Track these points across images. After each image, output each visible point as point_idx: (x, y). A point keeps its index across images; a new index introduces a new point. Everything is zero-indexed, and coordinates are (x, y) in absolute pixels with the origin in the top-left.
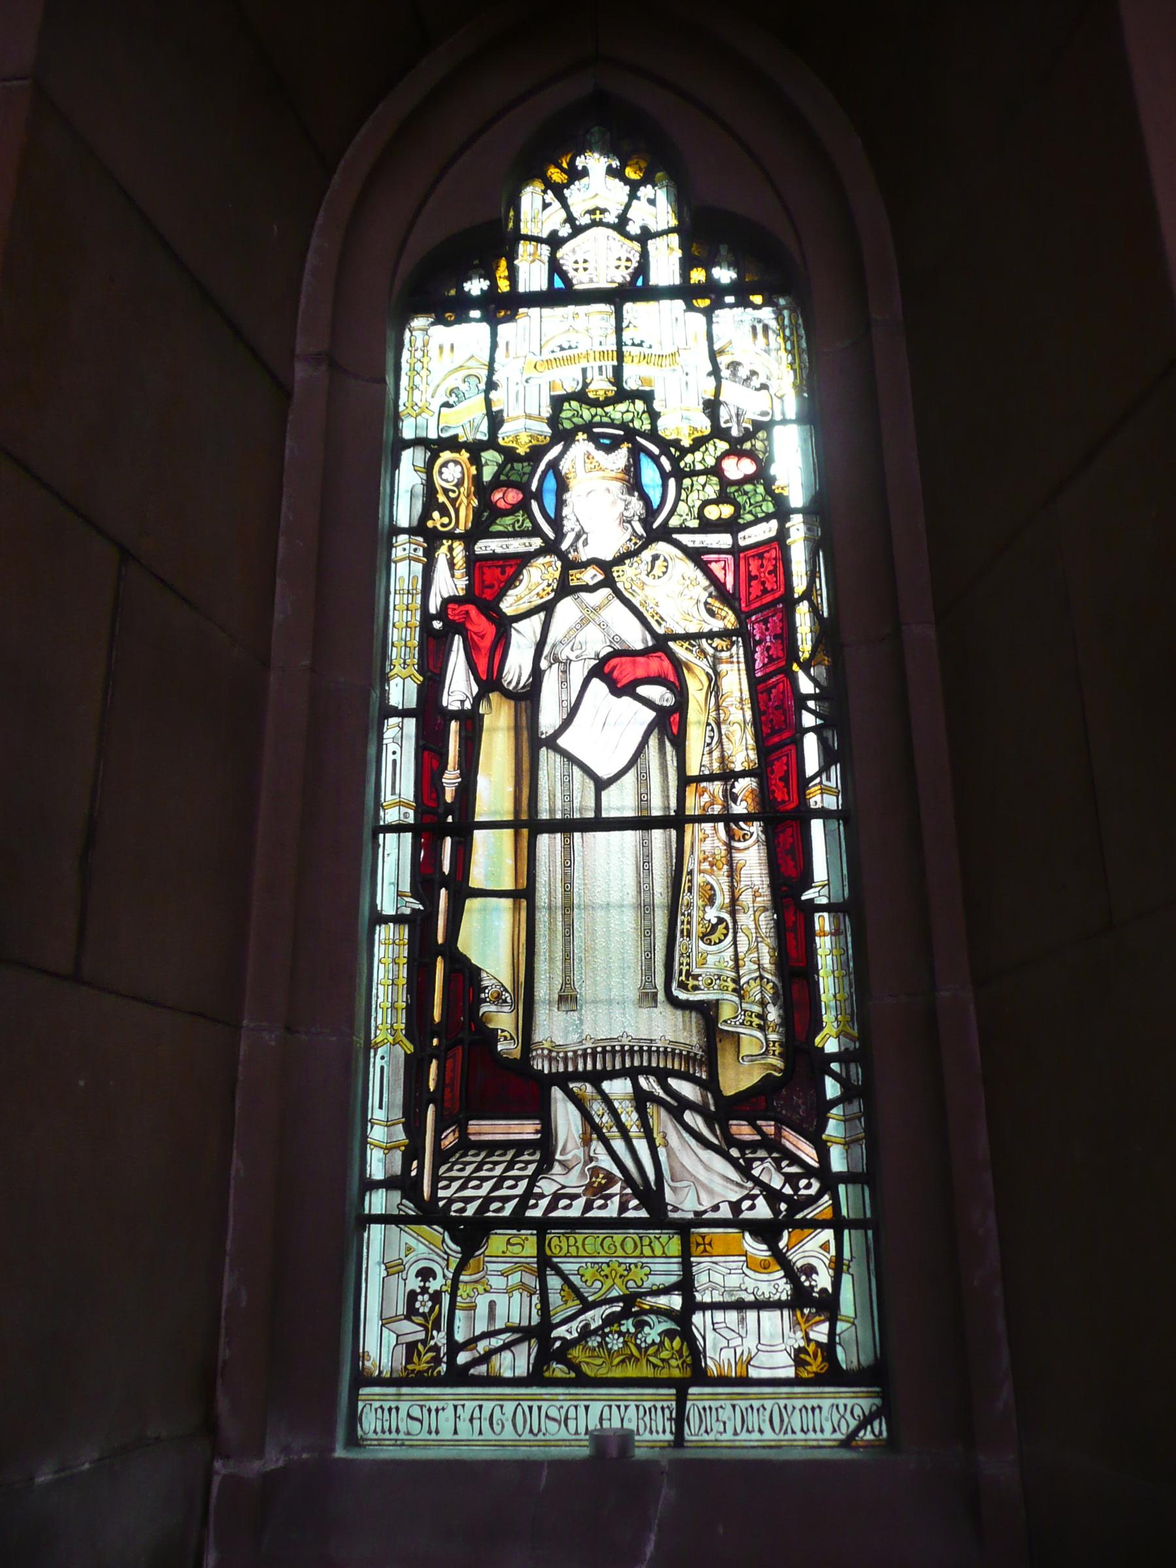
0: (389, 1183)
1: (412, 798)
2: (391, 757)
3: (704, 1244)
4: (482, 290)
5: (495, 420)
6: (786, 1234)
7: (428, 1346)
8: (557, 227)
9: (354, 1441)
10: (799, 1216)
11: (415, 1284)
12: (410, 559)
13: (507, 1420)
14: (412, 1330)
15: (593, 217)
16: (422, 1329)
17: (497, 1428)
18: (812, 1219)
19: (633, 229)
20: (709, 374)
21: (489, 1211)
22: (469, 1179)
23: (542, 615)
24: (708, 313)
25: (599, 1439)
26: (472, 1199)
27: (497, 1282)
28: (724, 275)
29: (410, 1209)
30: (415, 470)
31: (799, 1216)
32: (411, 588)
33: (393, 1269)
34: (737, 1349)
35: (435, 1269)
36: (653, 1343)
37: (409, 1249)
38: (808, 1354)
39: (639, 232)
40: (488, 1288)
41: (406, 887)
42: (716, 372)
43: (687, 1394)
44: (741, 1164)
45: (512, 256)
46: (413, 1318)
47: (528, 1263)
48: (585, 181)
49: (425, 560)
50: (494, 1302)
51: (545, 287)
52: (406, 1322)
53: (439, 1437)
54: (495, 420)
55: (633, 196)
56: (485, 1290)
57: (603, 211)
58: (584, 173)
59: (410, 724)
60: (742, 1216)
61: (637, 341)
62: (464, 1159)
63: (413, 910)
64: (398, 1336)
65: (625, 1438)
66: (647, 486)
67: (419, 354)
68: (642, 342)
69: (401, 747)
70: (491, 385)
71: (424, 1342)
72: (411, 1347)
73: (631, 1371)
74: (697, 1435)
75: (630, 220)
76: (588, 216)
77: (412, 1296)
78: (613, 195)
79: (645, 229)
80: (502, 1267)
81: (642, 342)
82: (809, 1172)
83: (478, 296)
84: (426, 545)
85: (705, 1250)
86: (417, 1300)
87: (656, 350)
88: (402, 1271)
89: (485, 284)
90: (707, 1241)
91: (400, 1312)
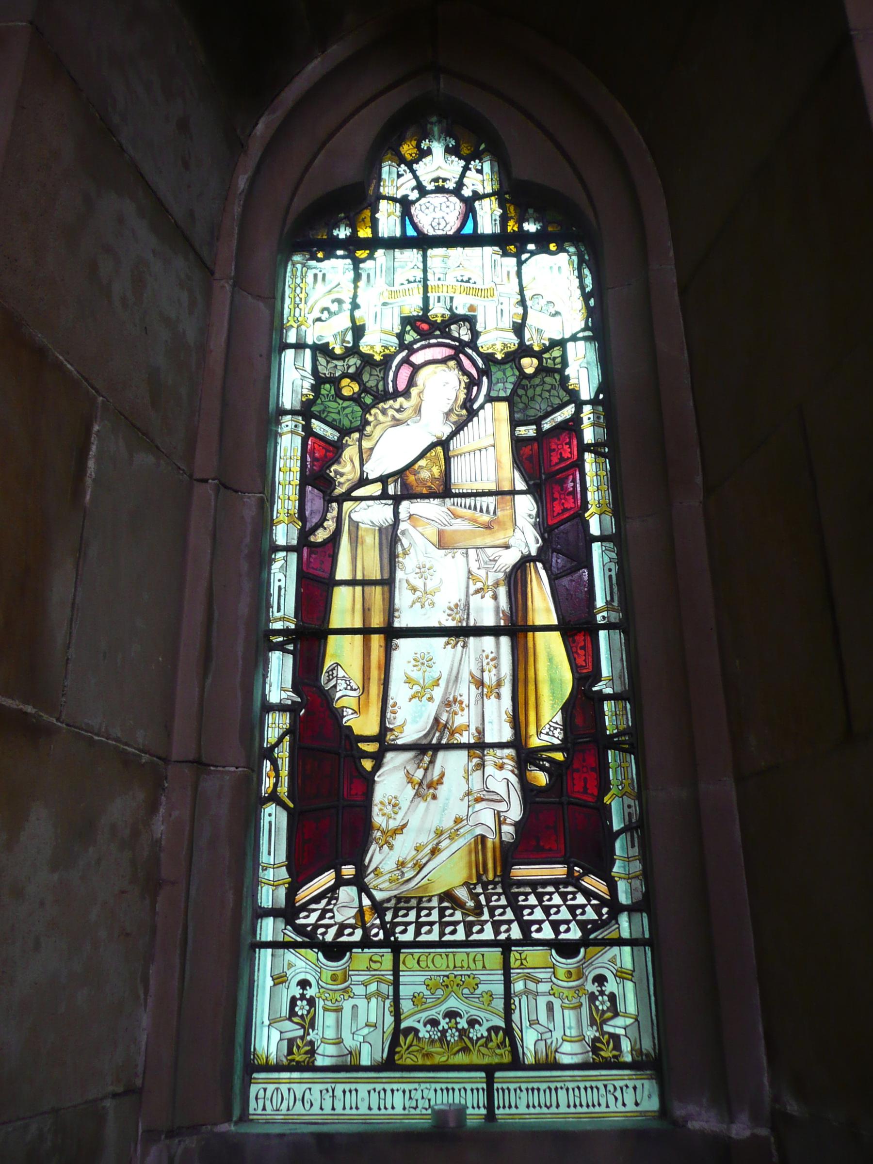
0: (274, 912)
1: (293, 615)
2: (277, 584)
3: (521, 960)
4: (346, 235)
6: (582, 950)
7: (305, 1042)
8: (408, 192)
9: (244, 1117)
10: (592, 936)
11: (297, 992)
12: (292, 432)
13: (316, 1100)
14: (293, 1030)
15: (436, 184)
16: (299, 1027)
17: (307, 1106)
18: (603, 939)
19: (467, 192)
25: (440, 1116)
27: (359, 990)
29: (292, 936)
30: (296, 368)
31: (592, 936)
32: (292, 454)
33: (279, 980)
34: (547, 1041)
35: (312, 982)
36: (482, 1037)
37: (290, 965)
38: (603, 1043)
39: (471, 194)
40: (352, 995)
41: (288, 684)
42: (523, 302)
45: (375, 210)
46: (293, 1019)
47: (383, 975)
48: (429, 158)
49: (303, 433)
50: (356, 1006)
51: (398, 234)
52: (287, 1022)
53: (359, 1112)
55: (466, 168)
56: (349, 997)
57: (444, 180)
58: (429, 152)
59: (293, 557)
60: (560, 937)
61: (465, 279)
63: (293, 702)
64: (281, 1033)
65: (460, 1111)
67: (298, 281)
68: (470, 279)
69: (285, 576)
70: (355, 306)
71: (302, 1038)
72: (291, 1042)
73: (461, 1059)
74: (278, 1110)
75: (465, 185)
76: (433, 183)
77: (293, 1001)
78: (451, 168)
80: (362, 978)
81: (470, 279)
82: (603, 902)
83: (342, 239)
84: (304, 423)
85: (522, 964)
86: (609, 1001)
87: (479, 285)
88: (285, 982)
89: (348, 232)
90: (523, 956)
91: (283, 1014)
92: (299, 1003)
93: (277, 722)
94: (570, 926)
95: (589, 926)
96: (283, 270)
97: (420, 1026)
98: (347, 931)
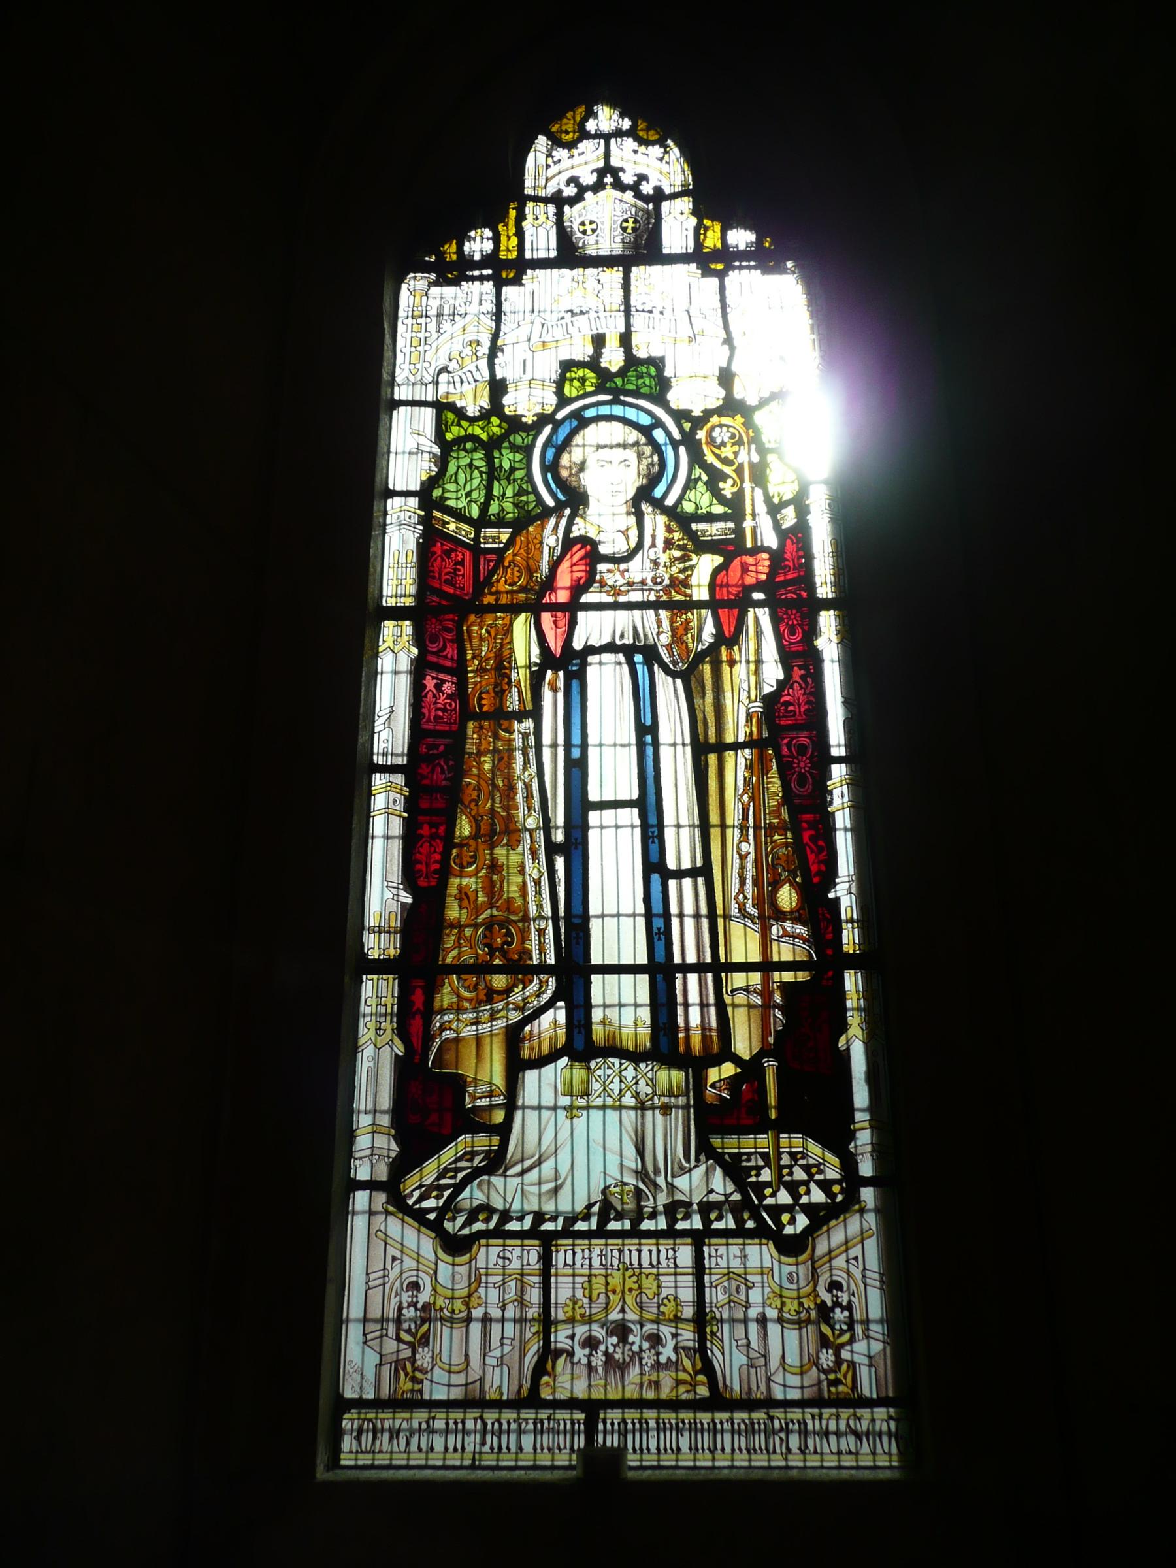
5: (498, 388)
22: (432, 1188)
24: (721, 275)
28: (741, 238)
39: (651, 192)
54: (498, 388)
79: (658, 190)
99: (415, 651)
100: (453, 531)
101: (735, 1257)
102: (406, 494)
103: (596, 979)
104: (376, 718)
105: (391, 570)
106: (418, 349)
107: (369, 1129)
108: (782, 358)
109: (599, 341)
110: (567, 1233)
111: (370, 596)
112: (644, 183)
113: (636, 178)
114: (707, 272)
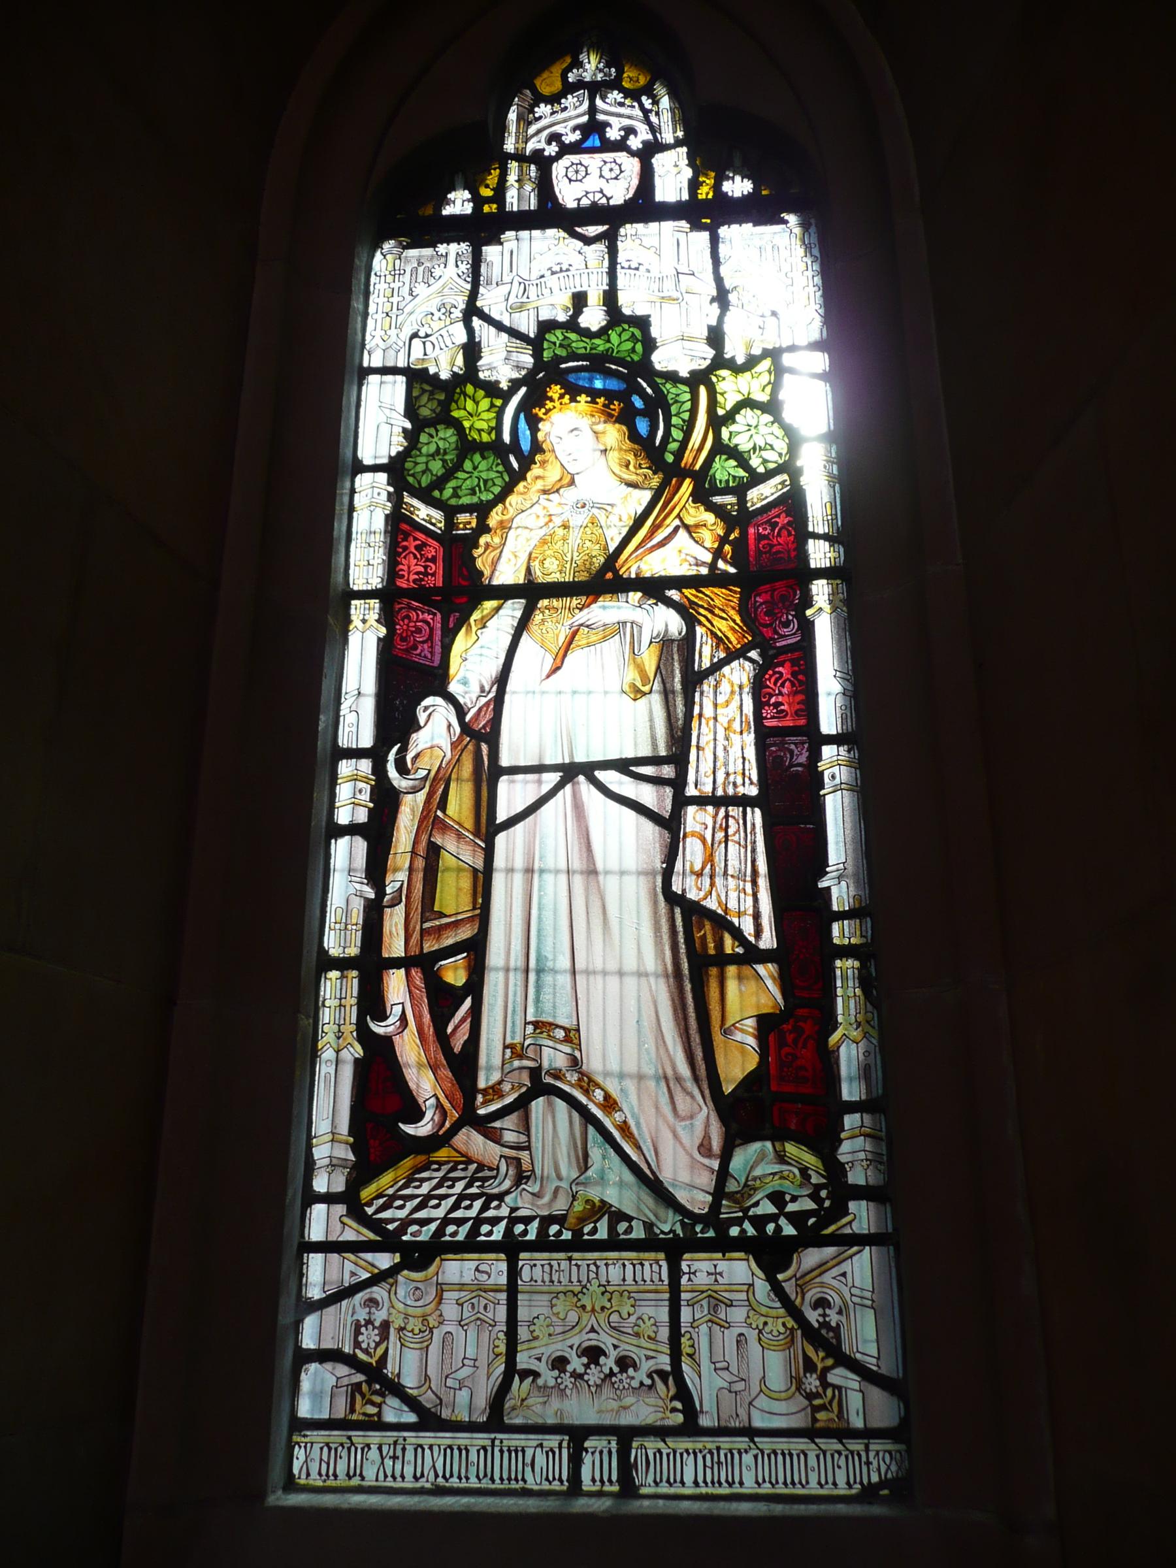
20: (713, 300)
21: (480, 1235)
22: (428, 1197)
23: (597, 773)
26: (428, 1221)
28: (738, 187)
39: (640, 146)
43: (839, 911)
44: (725, 573)
62: (451, 1175)
66: (745, 1150)
92: (363, 1330)
93: (344, 921)
94: (780, 1222)
95: (812, 1221)
96: (355, 388)
97: (542, 1367)
98: (495, 1203)
99: (383, 631)
100: (423, 519)
101: (715, 1266)
102: (375, 468)
103: (811, 541)
104: (343, 699)
105: (358, 550)
106: (391, 300)
107: (329, 1137)
108: (774, 314)
109: (579, 300)
110: (543, 1244)
111: (331, 591)
112: (632, 137)
113: (622, 133)
114: (696, 226)
